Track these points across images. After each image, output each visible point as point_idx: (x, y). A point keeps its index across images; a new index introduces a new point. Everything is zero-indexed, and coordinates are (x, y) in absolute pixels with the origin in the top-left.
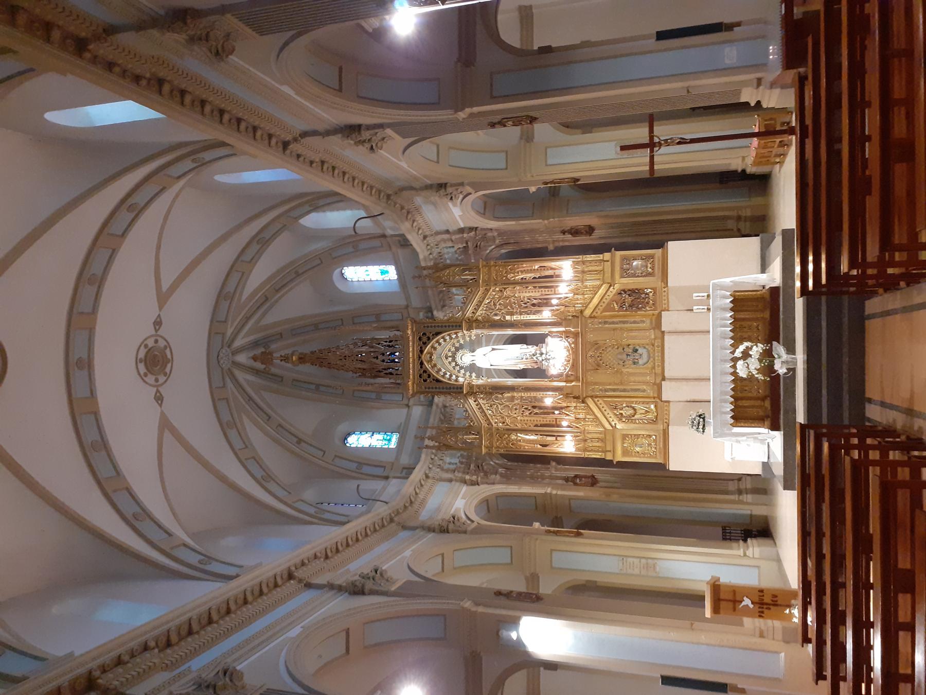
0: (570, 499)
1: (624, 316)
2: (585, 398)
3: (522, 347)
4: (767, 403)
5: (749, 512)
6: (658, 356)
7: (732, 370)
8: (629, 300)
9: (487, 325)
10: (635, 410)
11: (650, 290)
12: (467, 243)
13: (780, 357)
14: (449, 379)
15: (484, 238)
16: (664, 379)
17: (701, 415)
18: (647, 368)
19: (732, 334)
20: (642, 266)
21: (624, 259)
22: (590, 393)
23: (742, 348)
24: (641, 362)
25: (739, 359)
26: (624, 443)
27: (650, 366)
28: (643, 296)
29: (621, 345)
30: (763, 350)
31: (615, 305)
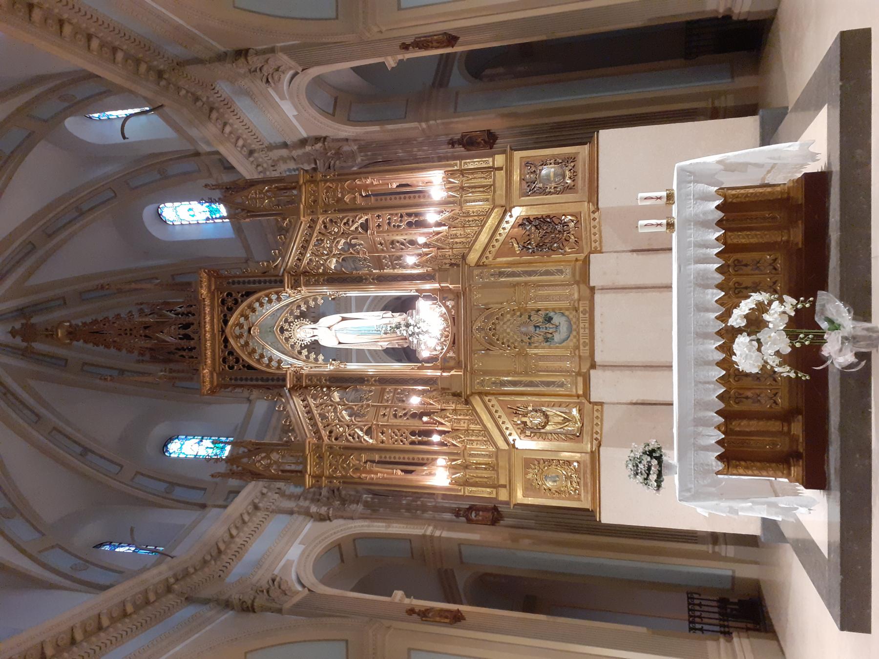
0: (461, 543)
1: (530, 263)
2: (468, 397)
3: (384, 316)
4: (797, 428)
5: (730, 573)
6: (585, 328)
7: (720, 356)
8: (536, 235)
9: (321, 280)
10: (546, 416)
11: (570, 217)
12: (316, 164)
13: (835, 326)
14: (268, 366)
15: (338, 154)
16: (593, 366)
17: (653, 451)
18: (567, 348)
19: (720, 278)
20: (556, 175)
21: (527, 163)
22: (477, 388)
23: (746, 306)
24: (557, 337)
25: (739, 331)
26: (526, 474)
27: (571, 344)
28: (559, 227)
29: (526, 310)
30: (797, 310)
31: (515, 245)
